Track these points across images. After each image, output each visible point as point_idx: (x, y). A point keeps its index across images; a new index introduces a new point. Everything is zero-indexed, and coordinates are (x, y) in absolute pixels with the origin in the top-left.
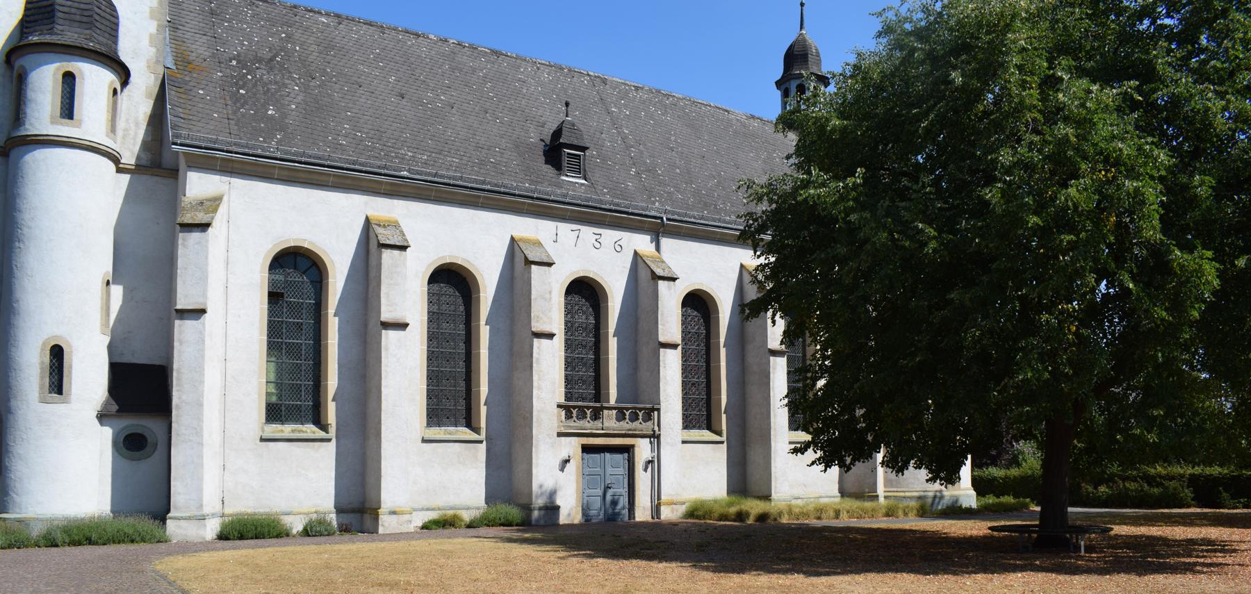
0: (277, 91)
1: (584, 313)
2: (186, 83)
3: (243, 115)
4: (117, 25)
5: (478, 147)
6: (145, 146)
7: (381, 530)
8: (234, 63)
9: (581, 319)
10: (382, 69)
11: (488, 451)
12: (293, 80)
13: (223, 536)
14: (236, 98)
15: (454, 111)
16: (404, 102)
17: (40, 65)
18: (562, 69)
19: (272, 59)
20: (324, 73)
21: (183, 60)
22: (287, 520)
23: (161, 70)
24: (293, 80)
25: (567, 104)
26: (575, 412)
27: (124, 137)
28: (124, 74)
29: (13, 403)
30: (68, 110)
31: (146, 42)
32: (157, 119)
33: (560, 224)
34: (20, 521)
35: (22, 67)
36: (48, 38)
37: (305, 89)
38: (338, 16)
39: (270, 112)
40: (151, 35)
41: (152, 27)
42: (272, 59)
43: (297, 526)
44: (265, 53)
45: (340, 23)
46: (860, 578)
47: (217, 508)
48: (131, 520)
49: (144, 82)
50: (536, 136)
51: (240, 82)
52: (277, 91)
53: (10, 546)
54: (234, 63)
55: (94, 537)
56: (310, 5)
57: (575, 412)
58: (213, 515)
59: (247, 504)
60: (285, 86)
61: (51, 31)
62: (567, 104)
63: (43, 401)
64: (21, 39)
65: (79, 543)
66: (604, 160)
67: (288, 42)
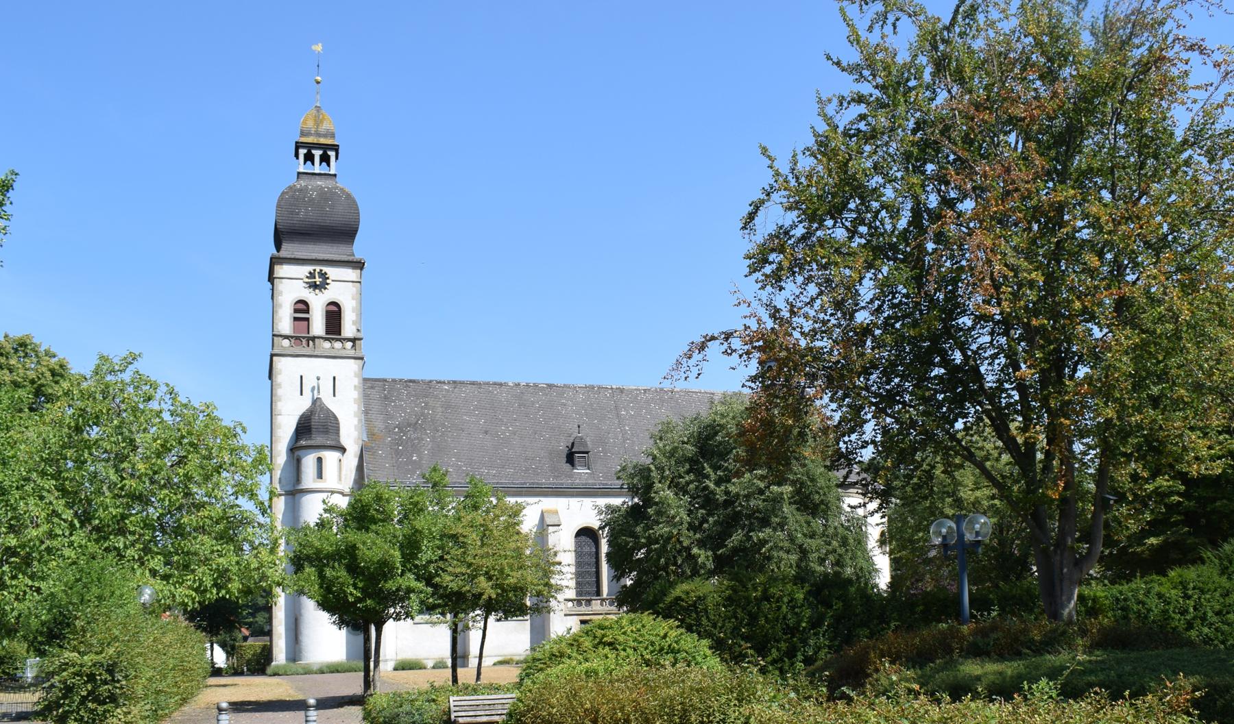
0: (419, 443)
1: (589, 546)
2: (373, 448)
3: (401, 462)
4: (339, 427)
5: (526, 459)
6: (356, 481)
7: (470, 666)
8: (397, 430)
9: (586, 549)
10: (477, 415)
11: (531, 625)
12: (427, 434)
13: (395, 669)
14: (397, 452)
15: (516, 437)
16: (487, 437)
17: (306, 455)
18: (593, 388)
19: (417, 423)
20: (443, 425)
21: (371, 434)
22: (425, 662)
23: (361, 442)
24: (427, 434)
25: (579, 427)
26: (583, 602)
27: (346, 478)
28: (343, 450)
29: (303, 611)
30: (320, 475)
31: (353, 429)
32: (360, 468)
33: (571, 499)
34: (307, 664)
35: (298, 456)
36: (309, 443)
37: (433, 438)
38: (455, 382)
39: (414, 458)
40: (355, 426)
41: (355, 421)
42: (417, 423)
43: (430, 664)
44: (413, 419)
45: (455, 388)
46: (471, 638)
47: (394, 657)
48: (355, 662)
49: (351, 460)
50: (563, 447)
51: (399, 442)
52: (419, 443)
53: (306, 674)
54: (397, 430)
55: (339, 669)
56: (439, 378)
57: (583, 602)
58: (391, 660)
59: (408, 655)
60: (422, 439)
61: (310, 438)
62: (579, 427)
63: (315, 610)
64: (296, 442)
65: (333, 672)
66: (605, 454)
67: (426, 408)
